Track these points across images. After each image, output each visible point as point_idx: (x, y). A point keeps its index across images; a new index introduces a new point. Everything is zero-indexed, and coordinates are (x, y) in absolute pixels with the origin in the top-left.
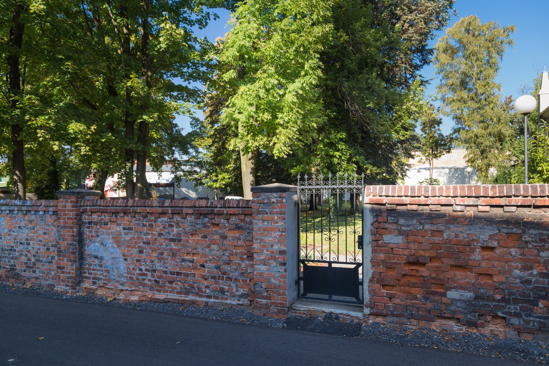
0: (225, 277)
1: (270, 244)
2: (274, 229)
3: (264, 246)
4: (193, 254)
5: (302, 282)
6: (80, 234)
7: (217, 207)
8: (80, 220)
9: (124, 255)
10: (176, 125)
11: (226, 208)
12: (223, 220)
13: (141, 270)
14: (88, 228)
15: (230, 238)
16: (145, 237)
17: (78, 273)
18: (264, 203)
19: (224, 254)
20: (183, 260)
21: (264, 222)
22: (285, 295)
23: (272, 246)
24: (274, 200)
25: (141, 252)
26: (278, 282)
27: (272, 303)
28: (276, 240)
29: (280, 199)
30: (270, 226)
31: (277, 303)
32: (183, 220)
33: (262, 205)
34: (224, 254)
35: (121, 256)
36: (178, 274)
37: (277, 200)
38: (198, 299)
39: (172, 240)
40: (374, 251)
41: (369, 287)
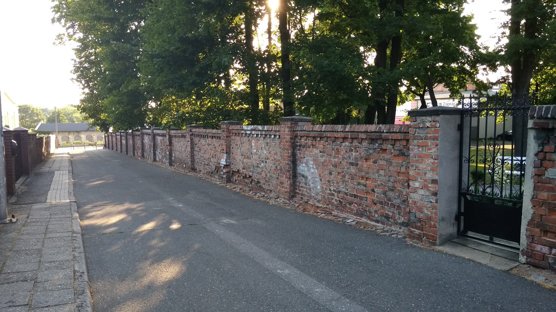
0: (390, 203)
1: (423, 171)
2: (428, 156)
3: (418, 174)
4: (366, 178)
5: (462, 218)
6: (294, 155)
7: (383, 132)
8: (294, 143)
9: (320, 176)
10: (509, 12)
11: (391, 132)
12: (389, 146)
13: (330, 190)
14: (299, 150)
15: (395, 164)
16: (333, 160)
17: (292, 188)
18: (419, 128)
19: (389, 181)
20: (359, 184)
21: (419, 148)
22: (436, 227)
23: (425, 174)
24: (428, 124)
25: (331, 174)
26: (429, 213)
27: (424, 235)
28: (429, 168)
29: (434, 123)
30: (424, 153)
31: (429, 235)
32: (359, 145)
33: (418, 130)
34: (389, 181)
35: (318, 176)
36: (355, 196)
37: (431, 125)
38: (369, 222)
39: (352, 164)
40: (535, 188)
41: (527, 230)
